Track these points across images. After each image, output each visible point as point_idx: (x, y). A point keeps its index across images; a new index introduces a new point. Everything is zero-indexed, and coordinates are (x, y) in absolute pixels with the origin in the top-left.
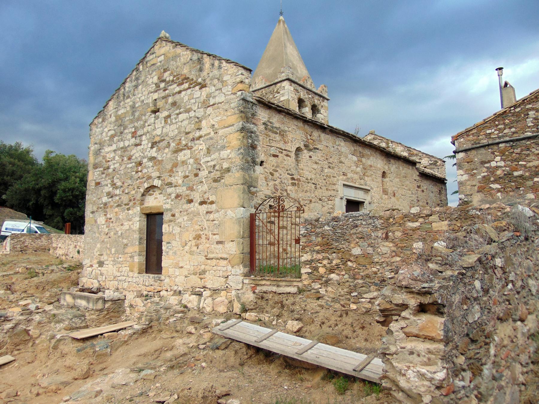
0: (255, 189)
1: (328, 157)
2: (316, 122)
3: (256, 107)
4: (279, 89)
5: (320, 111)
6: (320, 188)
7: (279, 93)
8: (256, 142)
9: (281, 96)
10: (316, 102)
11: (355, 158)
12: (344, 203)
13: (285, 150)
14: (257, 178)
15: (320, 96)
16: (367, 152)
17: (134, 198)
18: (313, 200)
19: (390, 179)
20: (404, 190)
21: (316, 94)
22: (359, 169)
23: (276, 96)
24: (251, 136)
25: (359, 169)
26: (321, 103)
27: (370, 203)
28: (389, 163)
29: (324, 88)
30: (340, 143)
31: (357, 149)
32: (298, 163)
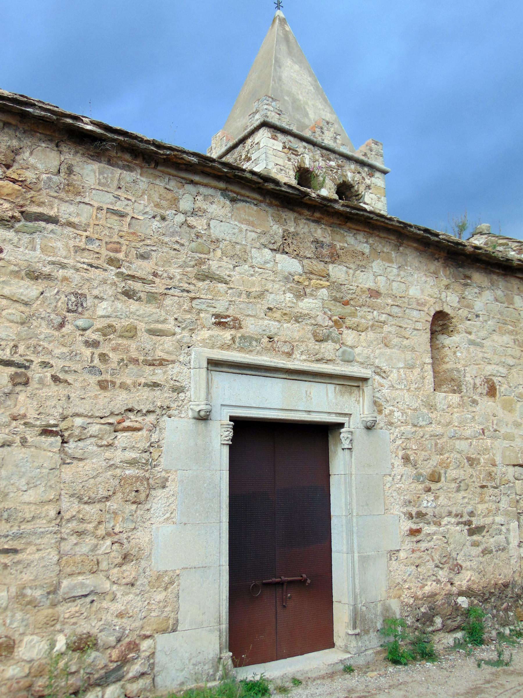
4: (251, 151)
6: (55, 379)
10: (350, 176)
15: (362, 164)
19: (472, 337)
21: (349, 158)
26: (363, 178)
27: (369, 428)
28: (466, 285)
29: (373, 145)
30: (200, 203)
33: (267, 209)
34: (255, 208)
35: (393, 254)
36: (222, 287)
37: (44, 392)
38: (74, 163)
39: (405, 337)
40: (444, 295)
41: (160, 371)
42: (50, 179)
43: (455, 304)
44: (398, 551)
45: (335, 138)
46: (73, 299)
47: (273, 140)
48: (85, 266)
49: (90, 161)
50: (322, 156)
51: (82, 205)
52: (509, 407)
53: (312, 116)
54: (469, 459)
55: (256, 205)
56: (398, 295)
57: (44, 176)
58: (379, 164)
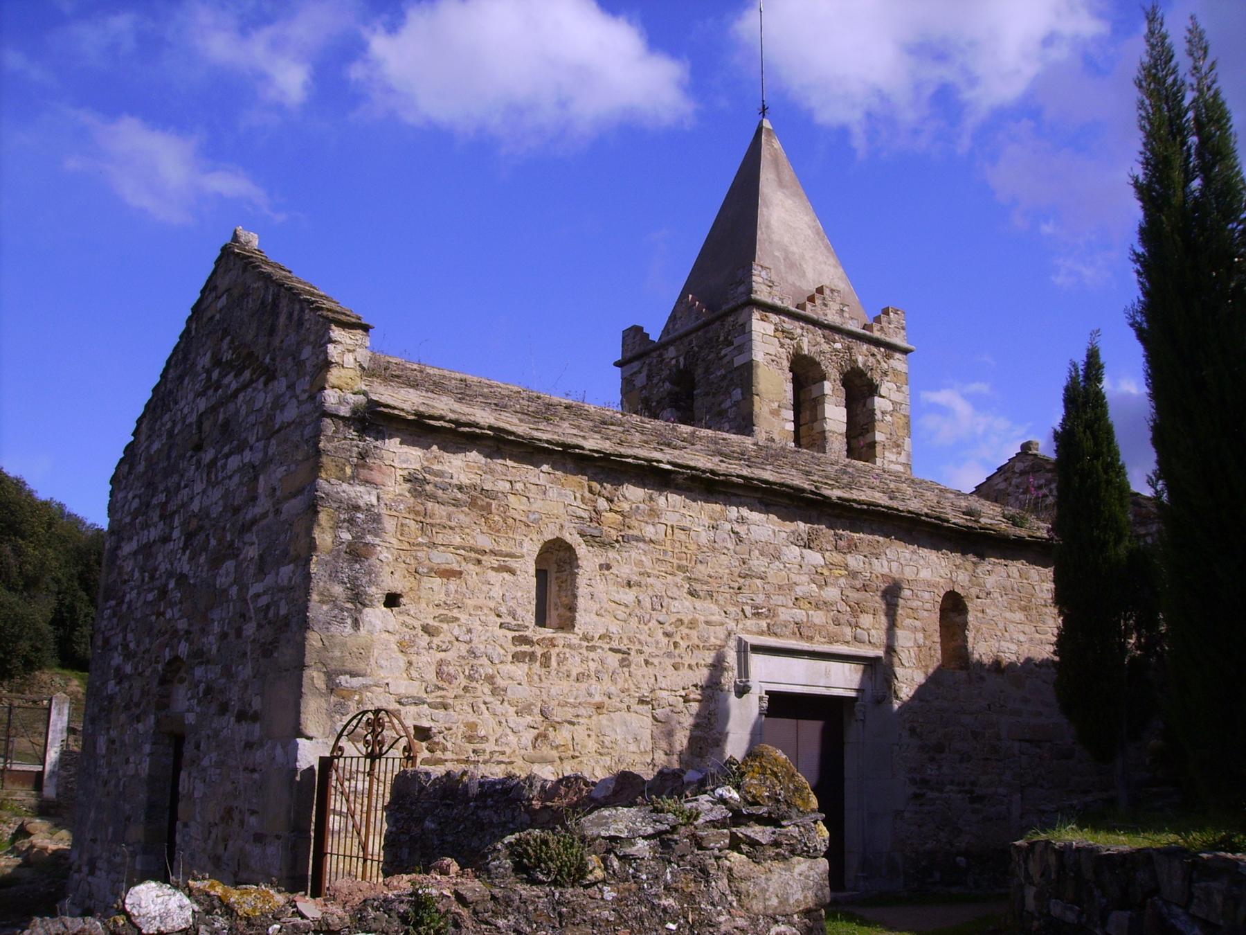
0: (356, 682)
8: (369, 538)
9: (736, 352)
13: (493, 553)
17: (629, 639)
22: (832, 593)
23: (723, 352)
24: (351, 521)
36: (759, 582)
43: (966, 584)
44: (903, 812)
45: (842, 310)
47: (763, 323)
48: (663, 574)
50: (824, 337)
53: (810, 274)
56: (910, 579)
57: (634, 506)
58: (899, 341)
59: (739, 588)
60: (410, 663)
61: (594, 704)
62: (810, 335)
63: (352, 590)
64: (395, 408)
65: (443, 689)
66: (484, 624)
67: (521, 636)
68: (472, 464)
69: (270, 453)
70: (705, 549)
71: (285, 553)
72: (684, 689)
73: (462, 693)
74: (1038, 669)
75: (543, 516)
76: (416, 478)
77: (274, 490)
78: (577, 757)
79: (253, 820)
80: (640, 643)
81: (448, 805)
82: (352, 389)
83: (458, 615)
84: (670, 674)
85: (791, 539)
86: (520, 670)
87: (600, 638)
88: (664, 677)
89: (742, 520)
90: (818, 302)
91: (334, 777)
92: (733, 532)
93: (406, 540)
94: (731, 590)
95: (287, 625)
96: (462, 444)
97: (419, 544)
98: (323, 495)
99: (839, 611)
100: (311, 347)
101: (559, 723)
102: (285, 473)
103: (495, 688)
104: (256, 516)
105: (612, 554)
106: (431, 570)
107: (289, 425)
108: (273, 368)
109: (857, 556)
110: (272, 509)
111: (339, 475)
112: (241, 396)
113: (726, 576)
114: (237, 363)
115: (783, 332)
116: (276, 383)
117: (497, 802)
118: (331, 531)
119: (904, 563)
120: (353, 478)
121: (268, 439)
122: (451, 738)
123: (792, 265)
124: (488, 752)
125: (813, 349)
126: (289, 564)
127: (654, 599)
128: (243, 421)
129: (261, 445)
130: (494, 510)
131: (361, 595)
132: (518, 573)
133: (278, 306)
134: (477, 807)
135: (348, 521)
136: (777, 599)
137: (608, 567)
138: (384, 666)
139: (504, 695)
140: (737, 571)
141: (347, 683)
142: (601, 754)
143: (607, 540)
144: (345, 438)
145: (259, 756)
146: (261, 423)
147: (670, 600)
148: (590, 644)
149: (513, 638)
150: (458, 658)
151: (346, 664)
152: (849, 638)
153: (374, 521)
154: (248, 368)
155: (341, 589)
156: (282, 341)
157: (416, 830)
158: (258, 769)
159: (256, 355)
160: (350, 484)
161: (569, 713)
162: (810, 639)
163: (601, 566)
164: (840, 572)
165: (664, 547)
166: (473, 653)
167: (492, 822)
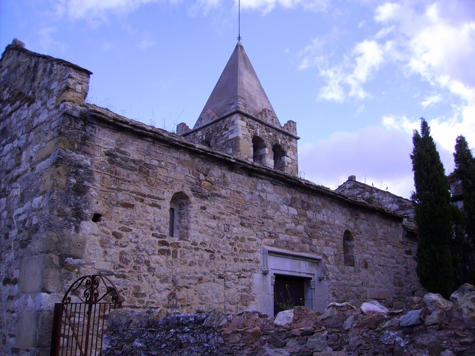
0: (76, 261)
1: (239, 209)
2: (213, 153)
3: (93, 127)
4: (228, 125)
5: (286, 152)
6: (222, 257)
7: (227, 129)
8: (86, 183)
9: (230, 133)
11: (293, 211)
12: (270, 280)
13: (150, 196)
14: (84, 242)
16: (315, 201)
18: (207, 277)
20: (383, 258)
22: (300, 228)
23: (224, 133)
24: (77, 173)
25: (300, 228)
31: (298, 196)
32: (181, 217)
33: (286, 188)
34: (282, 188)
35: (330, 205)
36: (271, 221)
37: (219, 262)
38: (225, 173)
39: (334, 242)
40: (348, 223)
41: (252, 255)
42: (218, 180)
43: (353, 227)
45: (273, 120)
46: (226, 227)
48: (230, 214)
49: (230, 172)
50: (266, 130)
51: (228, 190)
52: (373, 273)
53: (259, 105)
54: (357, 295)
55: (282, 186)
56: (331, 224)
57: (217, 179)
59: (263, 223)
60: (106, 252)
61: (198, 278)
62: (260, 128)
63: (76, 210)
64: (103, 114)
65: (123, 267)
66: (145, 234)
67: (163, 241)
68: (140, 150)
69: (30, 139)
70: (248, 203)
71: (37, 191)
72: (239, 271)
73: (133, 269)
74: (380, 267)
75: (174, 180)
76: (112, 154)
77: (31, 158)
78: (190, 305)
79: (12, 340)
80: (219, 247)
81: (152, 331)
82: (80, 103)
83: (131, 228)
84: (232, 263)
85: (284, 201)
86: (162, 259)
87: (201, 244)
88: (230, 265)
89: (263, 191)
90: (264, 115)
91: (64, 315)
92: (260, 196)
93: (106, 186)
94: (259, 224)
95: (37, 229)
96: (136, 139)
97: (112, 189)
98: (62, 157)
99: (304, 237)
100: (57, 82)
101: (181, 287)
102: (39, 148)
103: (150, 268)
104: (20, 173)
105: (206, 202)
106: (118, 203)
107: (42, 123)
108: (33, 97)
109: (311, 212)
110: (30, 169)
111: (71, 147)
112: (13, 115)
113: (257, 217)
114: (12, 99)
115: (250, 125)
116: (35, 104)
117: (193, 329)
118: (65, 177)
119: (329, 216)
120: (78, 150)
121: (29, 133)
122: (127, 294)
123: (252, 100)
124: (145, 302)
125: (261, 134)
126: (39, 196)
127: (226, 226)
128: (14, 127)
129: (24, 136)
130: (150, 174)
131: (81, 214)
132: (162, 208)
133: (37, 67)
134: (176, 333)
135: (75, 173)
136: (279, 230)
137: (205, 208)
138: (92, 253)
139: (154, 272)
140: (261, 215)
141: (71, 262)
142: (201, 304)
143: (204, 195)
144: (75, 128)
145: (16, 304)
146: (25, 125)
147: (233, 227)
148: (196, 247)
149: (159, 242)
150: (131, 250)
151: (71, 251)
152: (308, 250)
153: (89, 174)
154: (18, 100)
155: (70, 210)
156: (39, 83)
157: (127, 347)
158: (16, 311)
159: (23, 93)
160: (77, 153)
161: (186, 282)
162: (292, 249)
163: (201, 207)
164: (304, 218)
165: (230, 201)
166: (139, 248)
167: (189, 342)
